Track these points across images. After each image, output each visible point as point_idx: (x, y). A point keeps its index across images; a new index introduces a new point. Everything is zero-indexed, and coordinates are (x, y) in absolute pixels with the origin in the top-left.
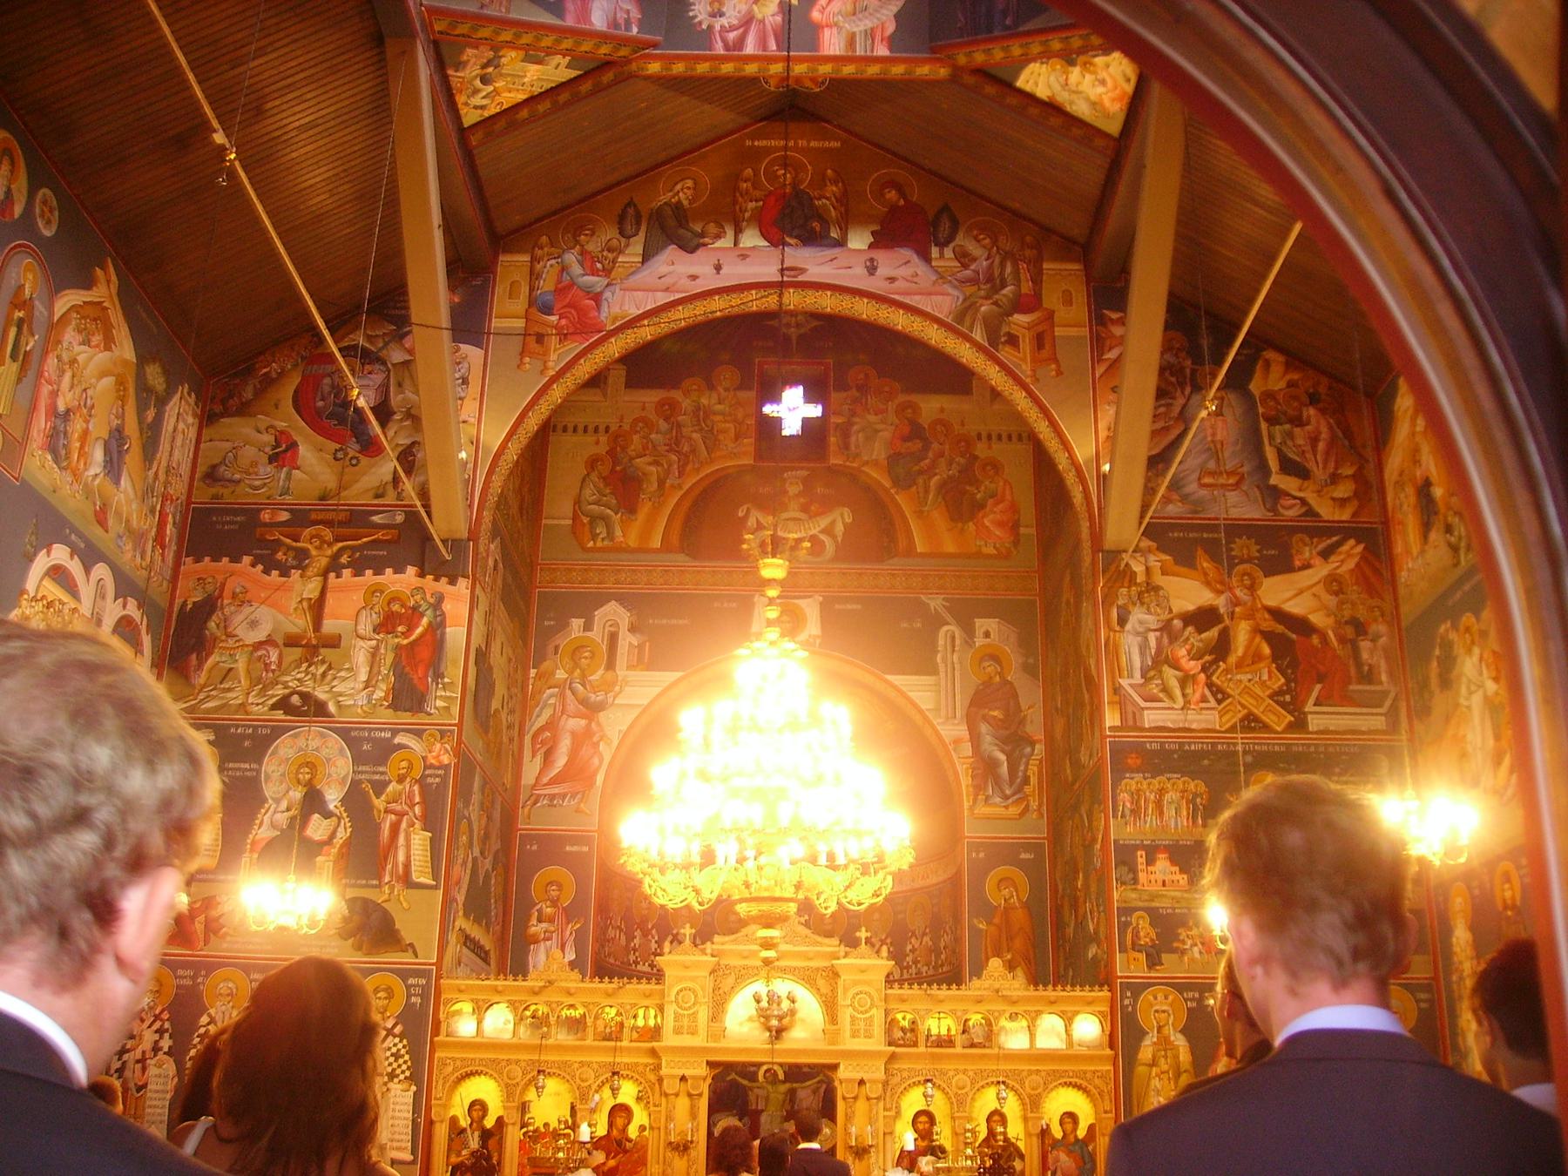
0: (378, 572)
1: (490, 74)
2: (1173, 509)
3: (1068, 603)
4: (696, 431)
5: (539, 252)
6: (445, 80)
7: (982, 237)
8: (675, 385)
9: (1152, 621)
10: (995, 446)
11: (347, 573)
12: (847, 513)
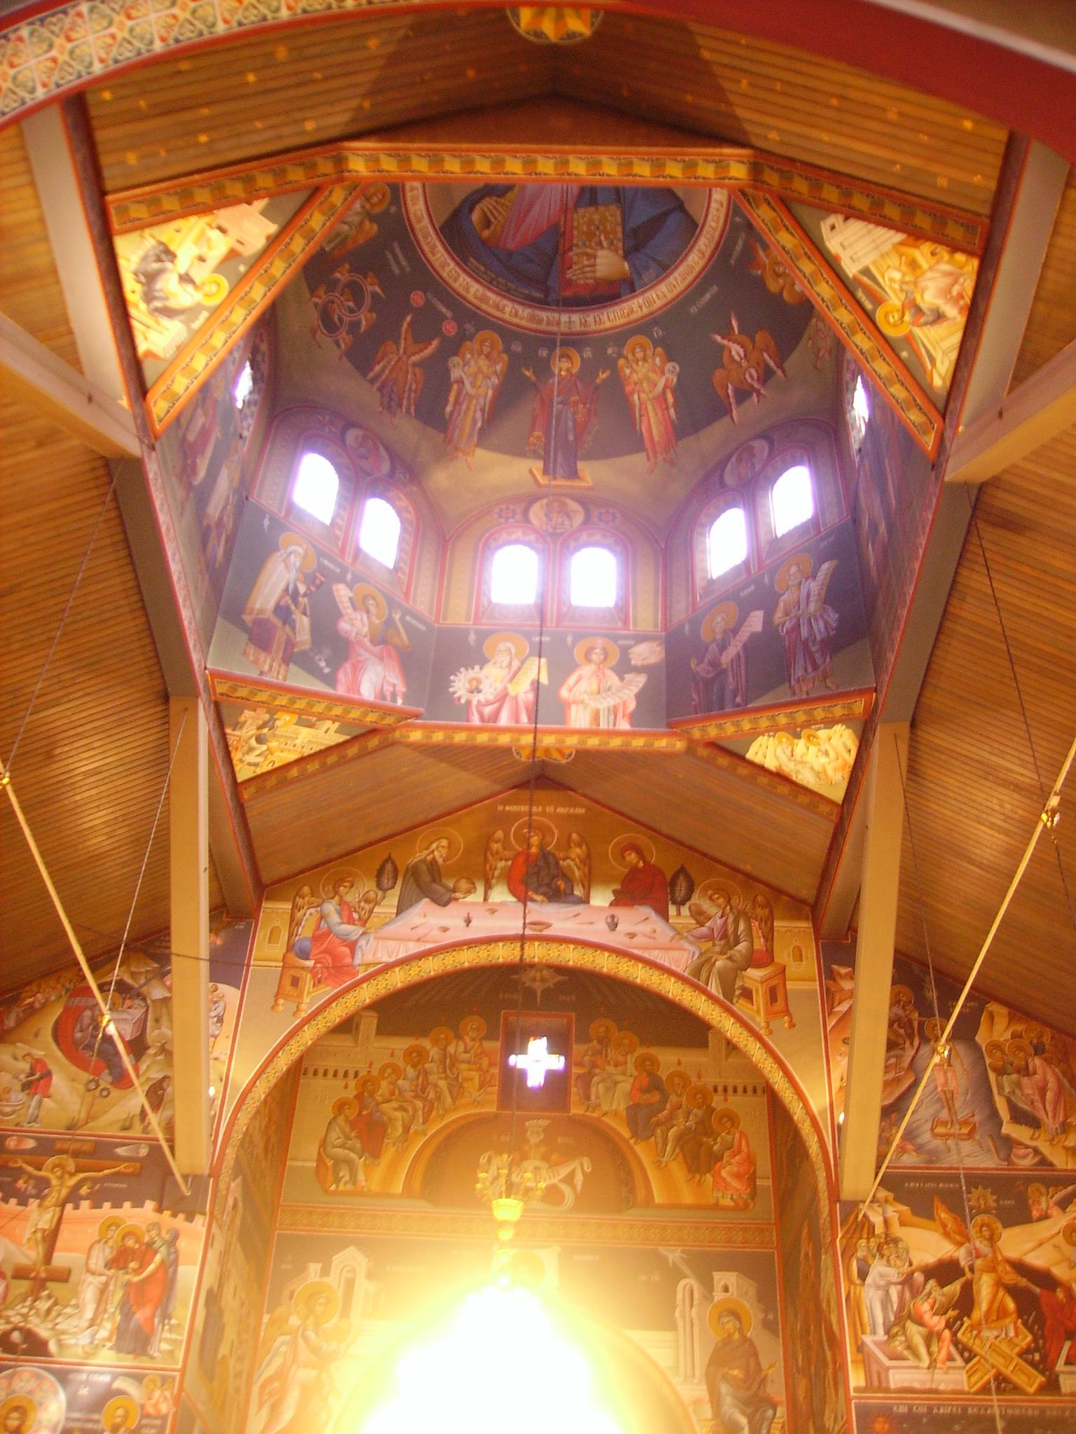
0: (117, 1205)
1: (265, 735)
2: (910, 1159)
3: (807, 1254)
4: (441, 1079)
5: (299, 901)
6: (224, 736)
7: (716, 896)
8: (423, 1033)
9: (893, 1274)
10: (732, 1098)
11: (85, 1204)
12: (586, 1162)
